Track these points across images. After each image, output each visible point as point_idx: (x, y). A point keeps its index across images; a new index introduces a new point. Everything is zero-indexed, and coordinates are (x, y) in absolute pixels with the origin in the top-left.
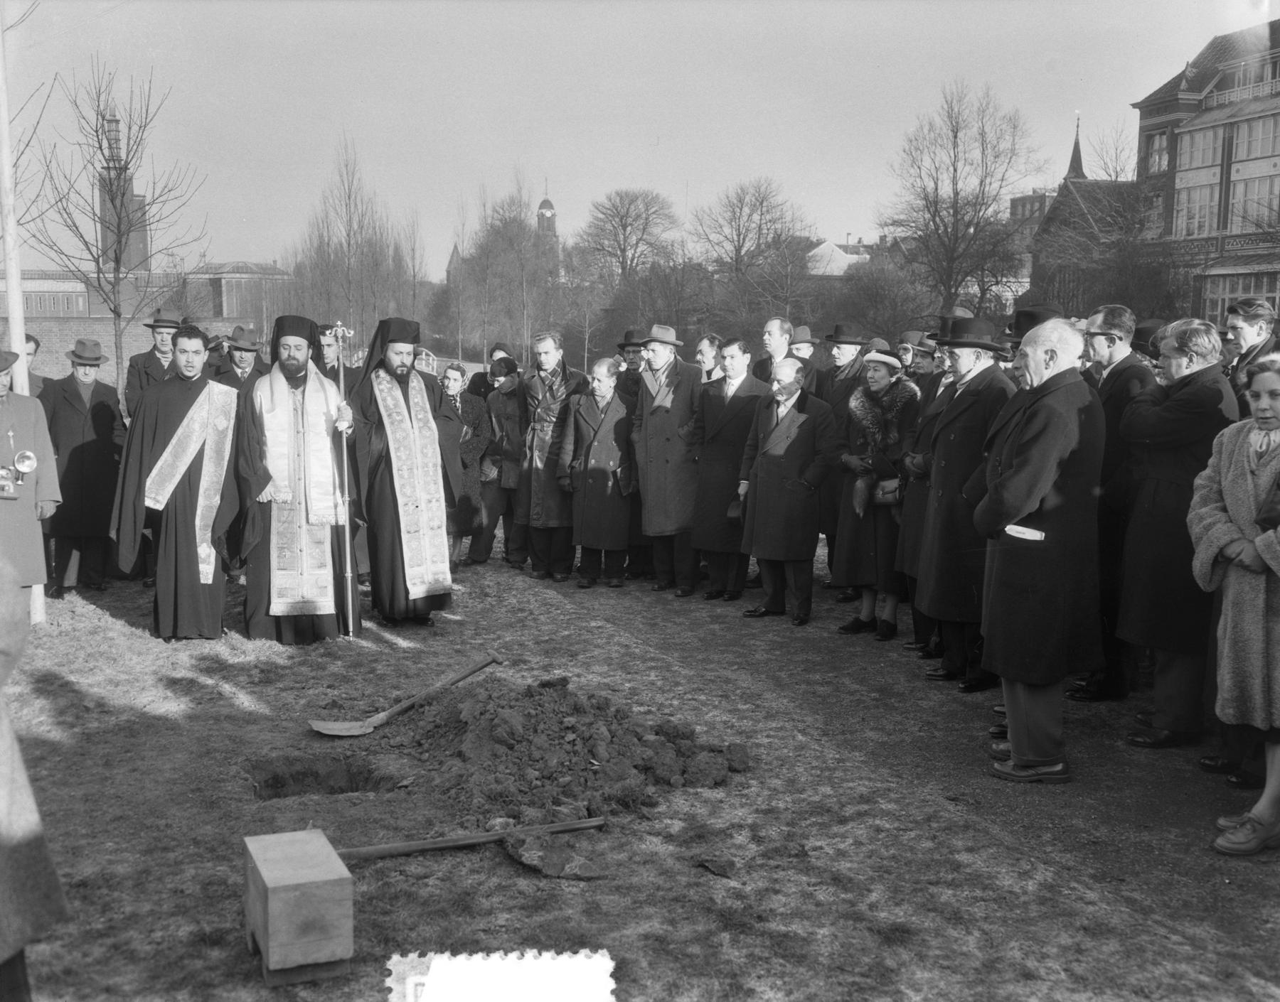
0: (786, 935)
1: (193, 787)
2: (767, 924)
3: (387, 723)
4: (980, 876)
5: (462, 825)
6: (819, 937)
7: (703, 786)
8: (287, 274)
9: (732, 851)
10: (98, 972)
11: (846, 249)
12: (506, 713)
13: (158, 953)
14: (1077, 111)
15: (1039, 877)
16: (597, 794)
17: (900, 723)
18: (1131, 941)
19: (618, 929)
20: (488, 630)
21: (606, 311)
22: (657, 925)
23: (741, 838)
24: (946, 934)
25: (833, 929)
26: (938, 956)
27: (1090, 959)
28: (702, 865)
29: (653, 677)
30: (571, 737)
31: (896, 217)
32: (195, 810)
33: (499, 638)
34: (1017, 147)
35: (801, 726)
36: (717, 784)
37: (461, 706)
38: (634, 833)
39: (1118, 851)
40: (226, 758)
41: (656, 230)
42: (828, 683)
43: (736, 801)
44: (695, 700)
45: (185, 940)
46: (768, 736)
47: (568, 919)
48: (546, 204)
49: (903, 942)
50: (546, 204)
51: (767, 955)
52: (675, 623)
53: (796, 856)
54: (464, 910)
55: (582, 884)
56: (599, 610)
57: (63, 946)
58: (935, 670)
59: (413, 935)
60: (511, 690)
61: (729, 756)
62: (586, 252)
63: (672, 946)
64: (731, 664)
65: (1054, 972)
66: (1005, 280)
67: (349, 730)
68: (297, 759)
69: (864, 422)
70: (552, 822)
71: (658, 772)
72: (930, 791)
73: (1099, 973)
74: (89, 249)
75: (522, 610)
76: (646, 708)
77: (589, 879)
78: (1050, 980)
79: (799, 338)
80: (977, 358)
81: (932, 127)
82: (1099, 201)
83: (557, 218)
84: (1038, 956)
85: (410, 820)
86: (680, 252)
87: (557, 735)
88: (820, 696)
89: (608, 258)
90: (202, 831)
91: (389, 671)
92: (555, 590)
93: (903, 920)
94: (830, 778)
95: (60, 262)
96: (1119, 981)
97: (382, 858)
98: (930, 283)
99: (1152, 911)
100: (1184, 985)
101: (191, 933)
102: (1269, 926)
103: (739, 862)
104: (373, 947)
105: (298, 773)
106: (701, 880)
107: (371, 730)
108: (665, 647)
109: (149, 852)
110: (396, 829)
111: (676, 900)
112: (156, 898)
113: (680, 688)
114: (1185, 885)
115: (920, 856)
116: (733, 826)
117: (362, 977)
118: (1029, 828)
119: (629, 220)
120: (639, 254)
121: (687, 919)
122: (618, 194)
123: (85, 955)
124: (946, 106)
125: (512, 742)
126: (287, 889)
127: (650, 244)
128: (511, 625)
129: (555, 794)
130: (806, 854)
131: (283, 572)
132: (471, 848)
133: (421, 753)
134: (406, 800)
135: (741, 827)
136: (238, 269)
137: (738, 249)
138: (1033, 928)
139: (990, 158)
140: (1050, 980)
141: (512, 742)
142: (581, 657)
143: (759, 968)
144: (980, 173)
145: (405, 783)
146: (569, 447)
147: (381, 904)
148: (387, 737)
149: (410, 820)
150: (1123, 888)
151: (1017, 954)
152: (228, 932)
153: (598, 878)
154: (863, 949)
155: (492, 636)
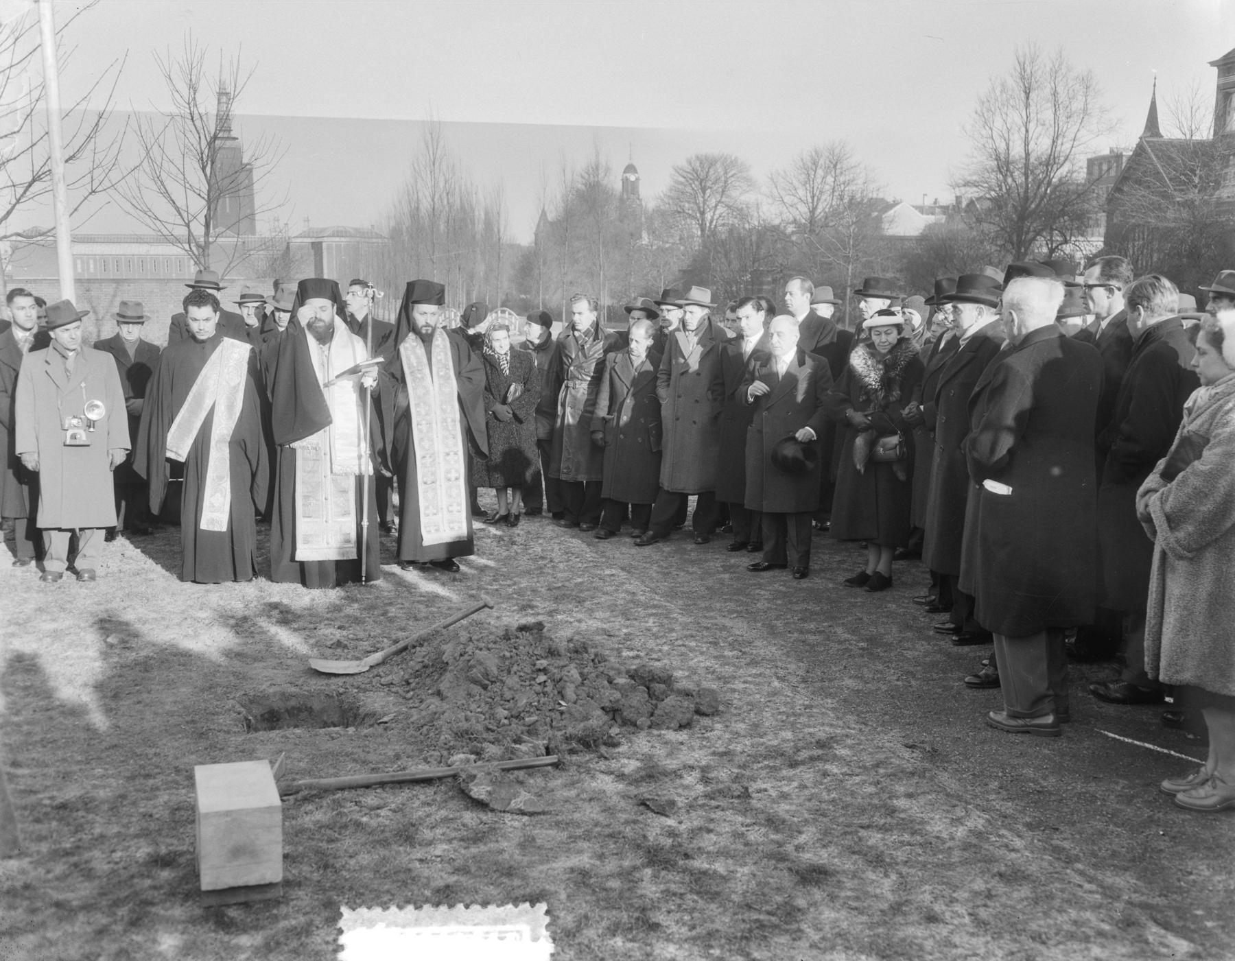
0: (705, 873)
1: (189, 719)
2: (692, 862)
3: (383, 663)
4: (912, 822)
5: (426, 760)
6: (739, 875)
7: (668, 728)
8: (381, 237)
9: (680, 791)
10: (52, 888)
11: (921, 209)
12: (481, 655)
13: (113, 871)
14: (1154, 71)
15: (970, 824)
16: (559, 734)
17: (881, 672)
18: (1043, 888)
19: (548, 861)
20: (506, 576)
21: (684, 271)
22: (586, 860)
23: (690, 779)
24: (863, 876)
25: (753, 868)
26: (849, 898)
27: (998, 904)
28: (643, 804)
29: (650, 624)
30: (542, 678)
31: (969, 178)
32: (185, 741)
33: (515, 584)
34: (1089, 106)
35: (782, 673)
36: (681, 727)
37: (444, 647)
38: (588, 771)
39: (1060, 801)
40: (225, 693)
41: (734, 193)
42: (821, 632)
43: (697, 744)
44: (683, 645)
45: (141, 861)
46: (745, 682)
47: (501, 852)
48: (631, 168)
49: (818, 883)
50: (631, 168)
51: (682, 891)
52: (688, 572)
53: (739, 797)
54: (406, 841)
55: (525, 819)
56: (618, 558)
57: (31, 863)
58: (943, 624)
59: (352, 862)
60: (491, 633)
61: (698, 700)
62: (668, 216)
63: (592, 881)
64: (730, 612)
65: (959, 916)
66: (1073, 239)
67: (345, 668)
68: (293, 695)
69: (867, 379)
70: (510, 759)
71: (625, 714)
72: (891, 740)
73: (1004, 918)
74: (180, 214)
75: (543, 558)
76: (636, 652)
77: (532, 814)
78: (952, 924)
79: (819, 299)
80: (979, 314)
81: (1004, 89)
82: (1173, 159)
83: (640, 182)
84: (947, 900)
85: (380, 754)
86: (756, 214)
87: (528, 677)
88: (809, 645)
89: (688, 220)
90: (186, 760)
91: (400, 614)
92: (581, 539)
93: (826, 861)
94: (793, 724)
95: (153, 227)
96: (1020, 927)
97: (342, 789)
98: (999, 243)
99: (1078, 859)
100: (1083, 932)
101: (148, 854)
102: (1192, 877)
103: (681, 802)
104: (312, 872)
105: (293, 708)
106: (640, 818)
107: (367, 668)
108: (672, 595)
109: (132, 778)
110: (364, 762)
111: (611, 836)
112: (125, 821)
113: (674, 634)
114: (1118, 836)
115: (860, 800)
116: (685, 767)
117: (293, 900)
118: (978, 776)
119: (709, 184)
120: (717, 215)
121: (617, 854)
122: (697, 157)
123: (48, 872)
124: (1018, 68)
125: (487, 682)
126: (218, 814)
127: (729, 207)
128: (529, 572)
129: (519, 732)
130: (749, 796)
131: (309, 519)
132: (428, 781)
133: (408, 692)
134: (381, 736)
135: (692, 768)
136: (338, 233)
137: (813, 211)
138: (951, 873)
139: (1062, 119)
140: (952, 924)
141: (487, 682)
142: (587, 604)
143: (671, 903)
144: (1052, 133)
145: (385, 719)
146: (604, 402)
147: (329, 832)
148: (379, 676)
149: (380, 754)
150: (1055, 837)
151: (927, 897)
152: (182, 854)
153: (543, 813)
154: (778, 889)
155: (509, 582)
